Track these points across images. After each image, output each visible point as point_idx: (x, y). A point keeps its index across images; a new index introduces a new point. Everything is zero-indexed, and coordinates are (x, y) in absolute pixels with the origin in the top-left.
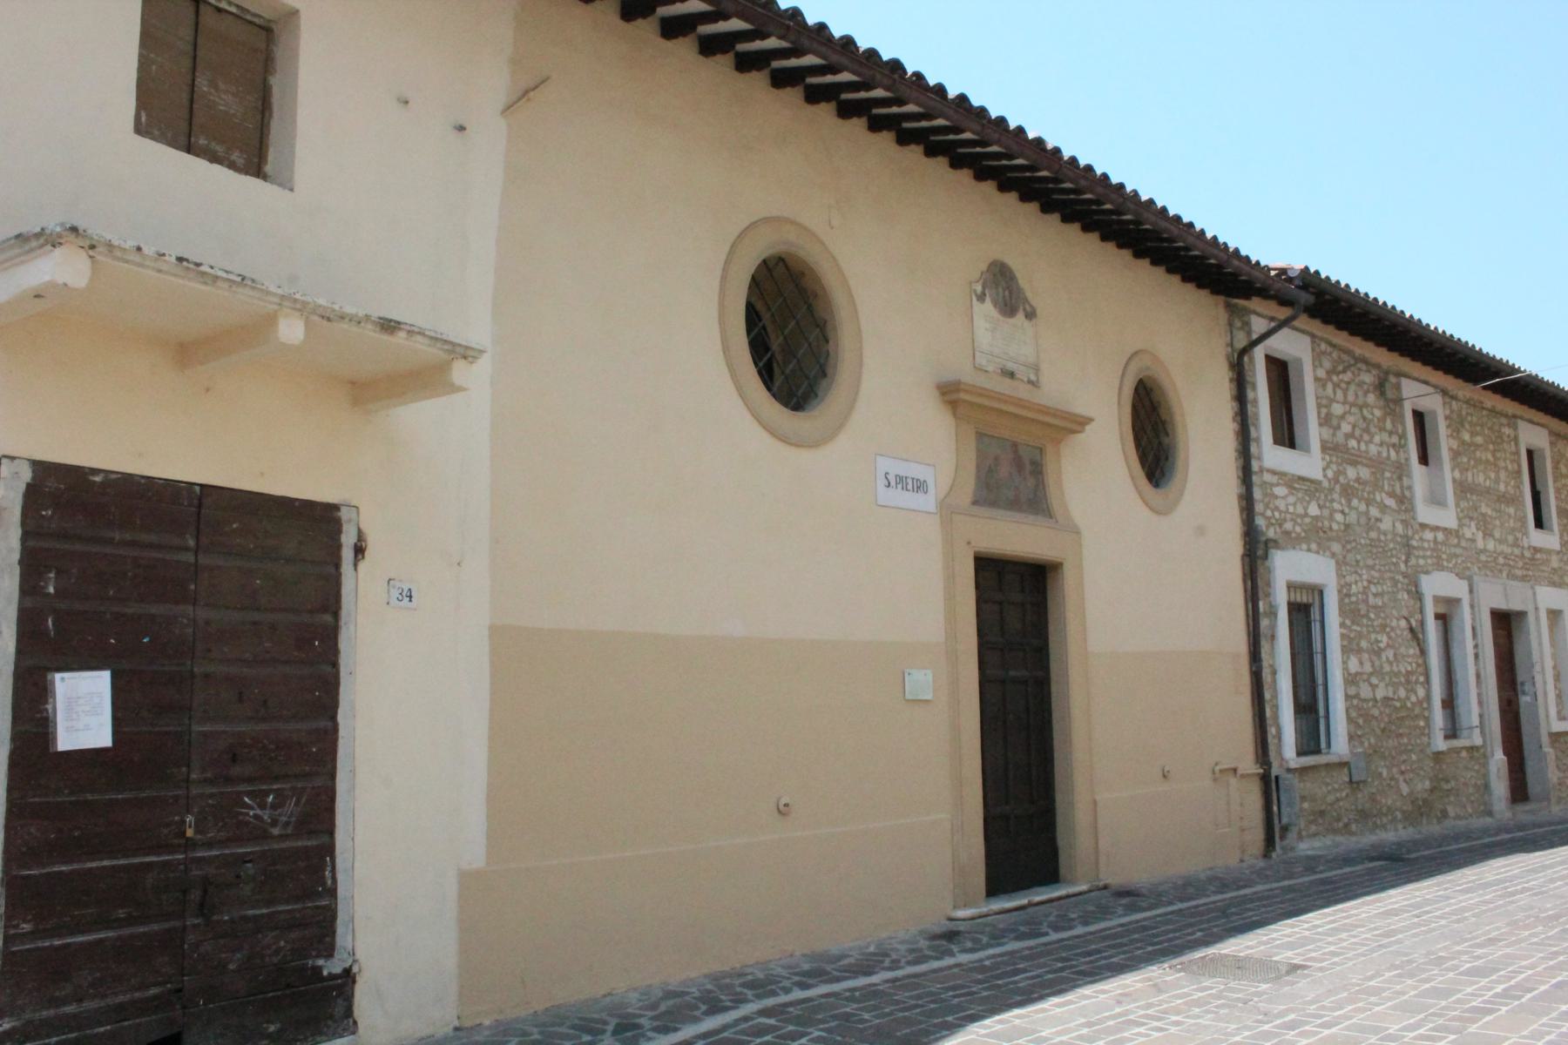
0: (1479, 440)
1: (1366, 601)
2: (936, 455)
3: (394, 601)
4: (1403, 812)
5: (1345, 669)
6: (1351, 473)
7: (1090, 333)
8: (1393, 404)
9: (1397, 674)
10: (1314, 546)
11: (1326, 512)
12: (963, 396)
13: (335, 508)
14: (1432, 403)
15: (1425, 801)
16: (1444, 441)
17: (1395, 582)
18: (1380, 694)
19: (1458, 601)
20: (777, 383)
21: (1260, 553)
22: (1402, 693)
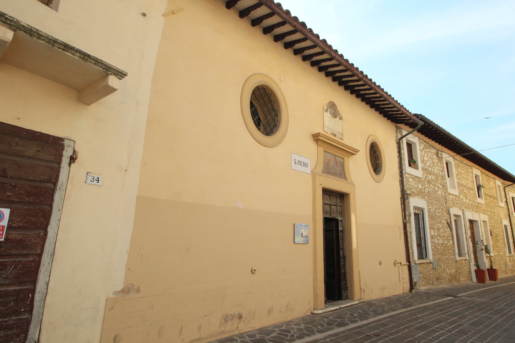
0: (463, 172)
1: (435, 214)
2: (312, 155)
3: (89, 181)
4: (448, 279)
5: (430, 234)
6: (430, 177)
7: (360, 125)
8: (440, 159)
9: (445, 236)
10: (420, 197)
11: (423, 188)
12: (320, 138)
13: (63, 139)
14: (450, 159)
15: (454, 275)
16: (454, 171)
17: (443, 209)
18: (440, 242)
19: (460, 216)
20: (262, 127)
21: (406, 197)
22: (446, 242)
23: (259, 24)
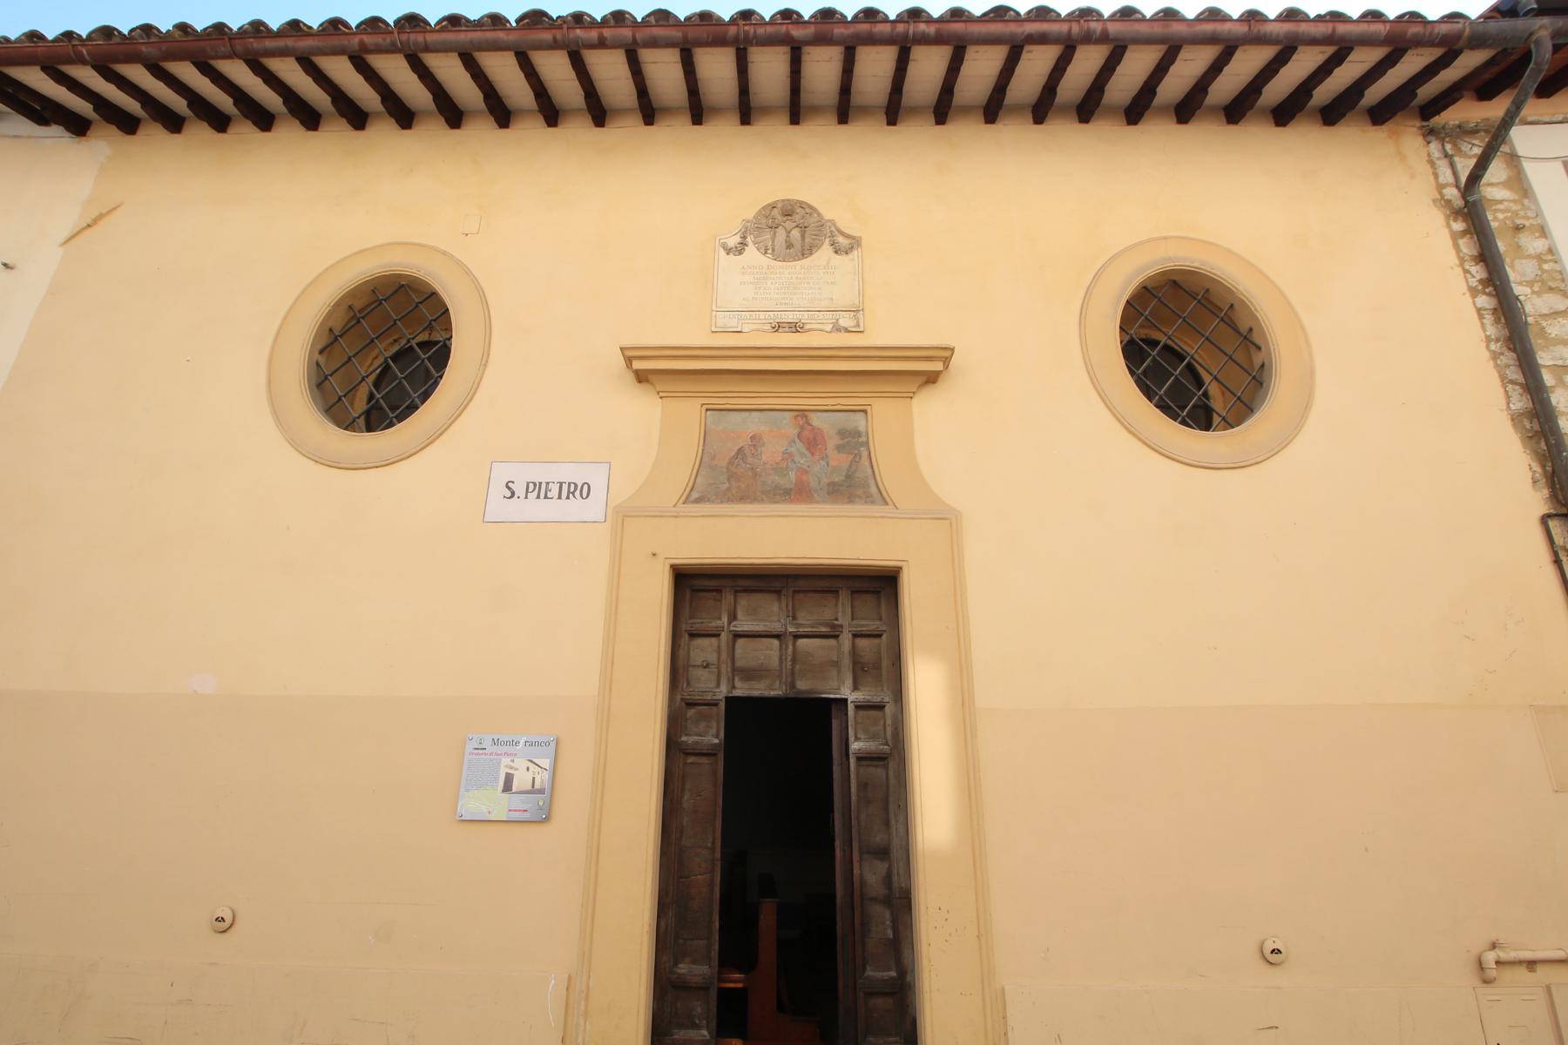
23: (1147, 106)
